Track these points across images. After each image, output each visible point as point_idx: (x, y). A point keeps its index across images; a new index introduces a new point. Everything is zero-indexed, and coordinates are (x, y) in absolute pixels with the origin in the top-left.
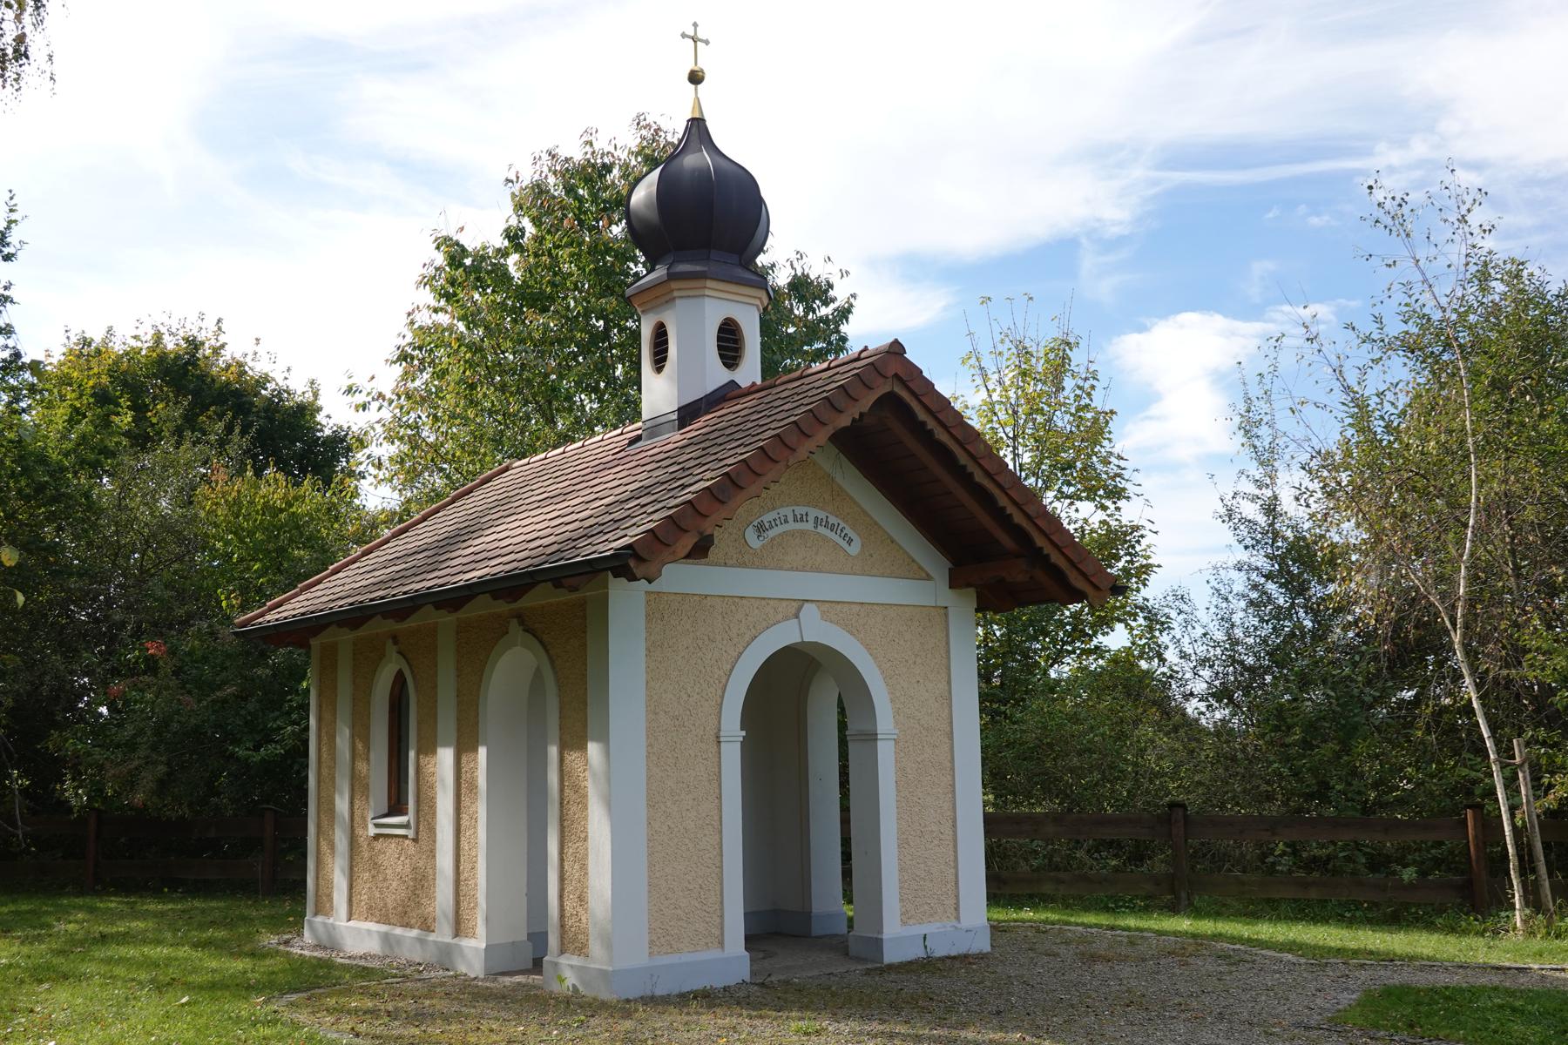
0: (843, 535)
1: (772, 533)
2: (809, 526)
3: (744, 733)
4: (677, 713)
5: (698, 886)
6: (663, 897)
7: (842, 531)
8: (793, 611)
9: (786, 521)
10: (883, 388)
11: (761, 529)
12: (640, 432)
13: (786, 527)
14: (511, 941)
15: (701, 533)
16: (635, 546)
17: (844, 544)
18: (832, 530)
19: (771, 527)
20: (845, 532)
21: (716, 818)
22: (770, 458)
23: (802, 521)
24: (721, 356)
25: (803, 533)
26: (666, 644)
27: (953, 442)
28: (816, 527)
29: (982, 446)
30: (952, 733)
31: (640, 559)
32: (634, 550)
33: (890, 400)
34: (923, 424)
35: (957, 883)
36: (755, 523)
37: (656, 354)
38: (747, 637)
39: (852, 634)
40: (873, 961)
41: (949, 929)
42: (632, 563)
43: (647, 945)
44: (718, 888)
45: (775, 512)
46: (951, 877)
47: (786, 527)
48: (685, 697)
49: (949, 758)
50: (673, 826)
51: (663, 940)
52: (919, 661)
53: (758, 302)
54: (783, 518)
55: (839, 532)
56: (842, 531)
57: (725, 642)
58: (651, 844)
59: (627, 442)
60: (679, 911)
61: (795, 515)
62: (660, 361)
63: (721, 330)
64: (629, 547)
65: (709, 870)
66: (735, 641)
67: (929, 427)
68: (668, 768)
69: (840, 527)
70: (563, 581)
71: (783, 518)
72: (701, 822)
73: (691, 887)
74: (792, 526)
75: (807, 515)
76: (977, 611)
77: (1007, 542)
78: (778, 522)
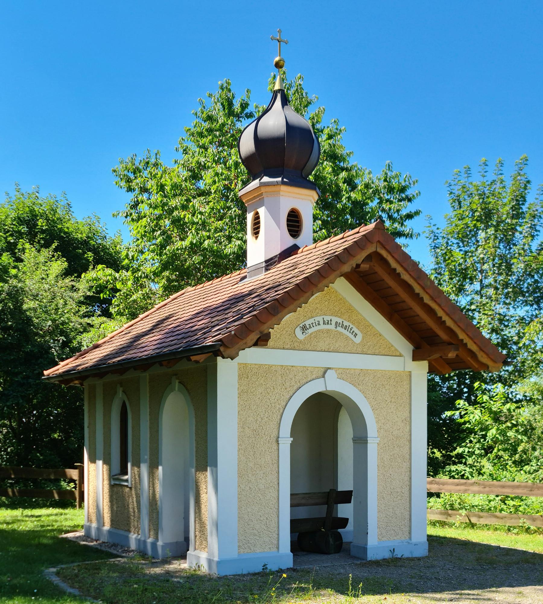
0: (351, 331)
1: (310, 331)
2: (332, 327)
3: (292, 439)
4: (254, 428)
5: (265, 518)
6: (246, 524)
7: (351, 329)
8: (322, 373)
9: (319, 324)
10: (370, 249)
11: (304, 329)
12: (246, 274)
13: (318, 328)
14: (176, 541)
15: (261, 332)
16: (223, 339)
17: (352, 337)
18: (345, 329)
19: (310, 327)
20: (353, 330)
21: (276, 483)
22: (302, 290)
23: (328, 323)
24: (289, 230)
25: (328, 331)
26: (249, 391)
27: (412, 280)
28: (336, 327)
29: (429, 283)
30: (411, 440)
31: (226, 347)
32: (222, 342)
33: (375, 257)
34: (395, 270)
35: (410, 519)
36: (301, 325)
37: (255, 229)
38: (295, 388)
39: (355, 386)
40: (361, 559)
41: (405, 543)
42: (222, 349)
43: (237, 548)
44: (276, 520)
45: (313, 319)
46: (407, 517)
47: (318, 328)
48: (260, 420)
49: (409, 453)
50: (252, 487)
51: (246, 546)
52: (393, 400)
53: (312, 199)
54: (317, 323)
55: (349, 330)
56: (351, 329)
57: (283, 390)
58: (240, 497)
59: (239, 279)
60: (255, 531)
61: (324, 321)
62: (256, 232)
63: (289, 215)
64: (220, 340)
65: (272, 510)
66: (288, 390)
67: (397, 272)
68: (250, 457)
69: (350, 328)
70: (191, 357)
71: (317, 323)
72: (268, 485)
73: (262, 519)
74: (322, 327)
75: (331, 320)
76: (428, 373)
77: (443, 336)
78: (314, 325)
